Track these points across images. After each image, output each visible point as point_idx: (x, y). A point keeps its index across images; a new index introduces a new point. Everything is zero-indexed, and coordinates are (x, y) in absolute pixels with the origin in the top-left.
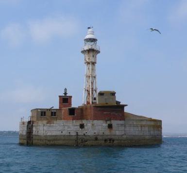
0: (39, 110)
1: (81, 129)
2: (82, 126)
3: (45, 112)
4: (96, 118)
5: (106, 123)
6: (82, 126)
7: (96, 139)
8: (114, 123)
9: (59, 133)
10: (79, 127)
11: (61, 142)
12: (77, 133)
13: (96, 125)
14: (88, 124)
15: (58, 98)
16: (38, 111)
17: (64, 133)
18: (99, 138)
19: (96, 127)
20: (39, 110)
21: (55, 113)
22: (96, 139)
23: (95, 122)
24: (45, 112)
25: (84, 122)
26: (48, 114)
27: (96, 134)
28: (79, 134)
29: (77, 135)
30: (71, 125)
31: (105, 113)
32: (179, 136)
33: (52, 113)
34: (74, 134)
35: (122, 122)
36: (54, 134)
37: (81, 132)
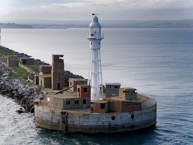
0: (65, 100)
1: (112, 121)
2: (113, 118)
3: (69, 102)
4: (123, 111)
5: (130, 114)
6: (113, 118)
7: (123, 127)
8: (135, 113)
9: (94, 124)
10: (111, 119)
11: (93, 132)
12: (110, 123)
13: (123, 116)
14: (118, 116)
15: (52, 56)
16: (64, 101)
17: (99, 124)
18: (126, 126)
19: (123, 118)
20: (65, 100)
21: (77, 101)
22: (123, 127)
23: (123, 114)
24: (69, 102)
25: (114, 114)
26: (73, 102)
27: (124, 123)
28: (111, 124)
29: (110, 125)
30: (104, 117)
31: (129, 106)
32: (104, 3)
33: (75, 101)
34: (107, 124)
35: (139, 112)
36: (90, 124)
37: (113, 123)
